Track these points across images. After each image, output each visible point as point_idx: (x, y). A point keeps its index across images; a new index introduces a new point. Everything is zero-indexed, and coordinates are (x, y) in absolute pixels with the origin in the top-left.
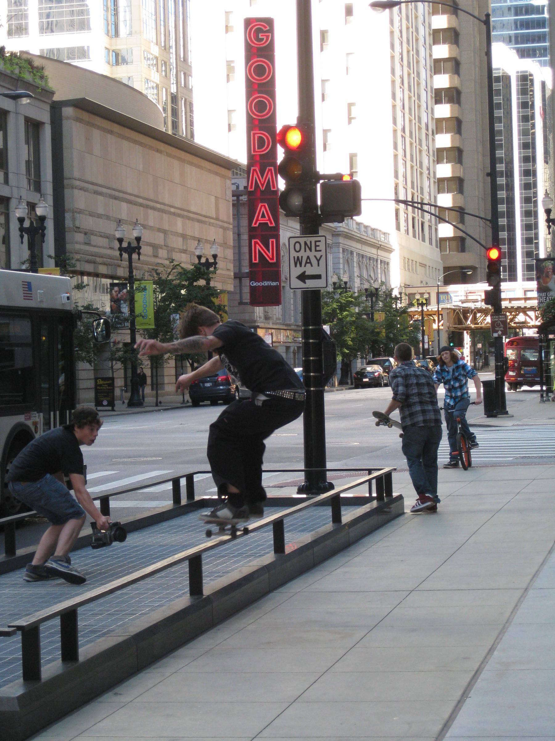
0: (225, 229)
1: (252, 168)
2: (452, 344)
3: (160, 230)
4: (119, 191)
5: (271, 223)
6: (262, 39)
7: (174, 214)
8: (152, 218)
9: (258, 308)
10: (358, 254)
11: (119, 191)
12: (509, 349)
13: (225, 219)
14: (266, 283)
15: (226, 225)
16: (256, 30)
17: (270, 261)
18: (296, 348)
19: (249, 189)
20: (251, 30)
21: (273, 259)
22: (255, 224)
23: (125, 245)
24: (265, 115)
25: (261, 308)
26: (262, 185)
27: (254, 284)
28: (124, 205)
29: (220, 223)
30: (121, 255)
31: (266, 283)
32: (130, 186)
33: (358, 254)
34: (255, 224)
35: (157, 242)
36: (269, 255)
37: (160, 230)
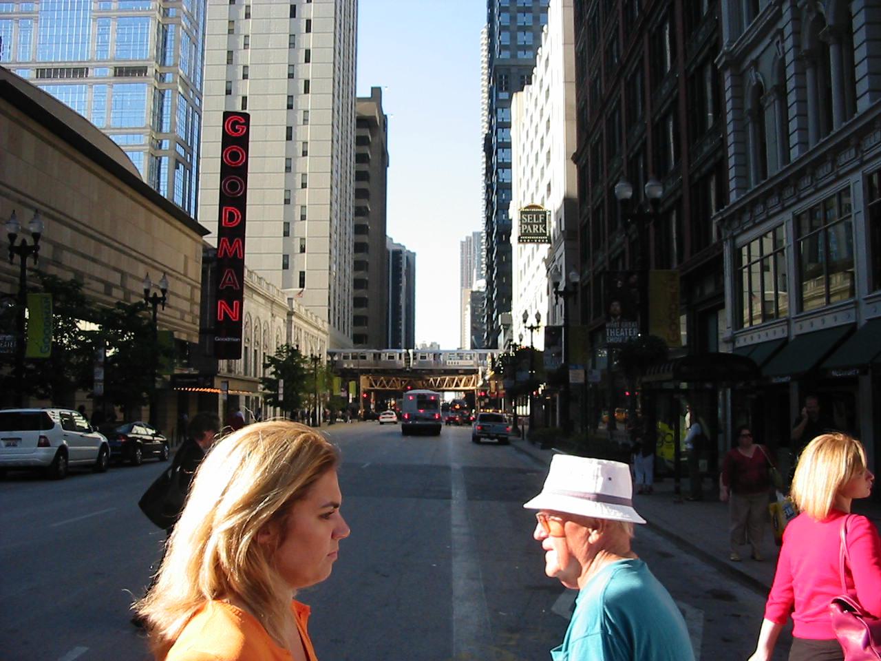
0: (193, 287)
1: (222, 239)
2: (144, 395)
3: (116, 269)
4: (61, 213)
5: (236, 286)
6: (238, 130)
7: (135, 258)
8: (107, 255)
9: (221, 361)
10: (305, 332)
11: (61, 213)
12: (95, 387)
13: (194, 278)
14: (228, 339)
15: (194, 283)
16: (234, 121)
17: (223, 302)
18: (254, 398)
19: (219, 257)
20: (241, 189)
21: (235, 318)
22: (222, 286)
23: (17, 243)
24: (228, 150)
25: (225, 361)
26: (230, 253)
27: (219, 340)
28: (68, 231)
29: (189, 280)
30: (12, 257)
31: (228, 339)
32: (77, 211)
33: (305, 332)
34: (222, 286)
35: (110, 280)
36: (233, 316)
37: (116, 269)
